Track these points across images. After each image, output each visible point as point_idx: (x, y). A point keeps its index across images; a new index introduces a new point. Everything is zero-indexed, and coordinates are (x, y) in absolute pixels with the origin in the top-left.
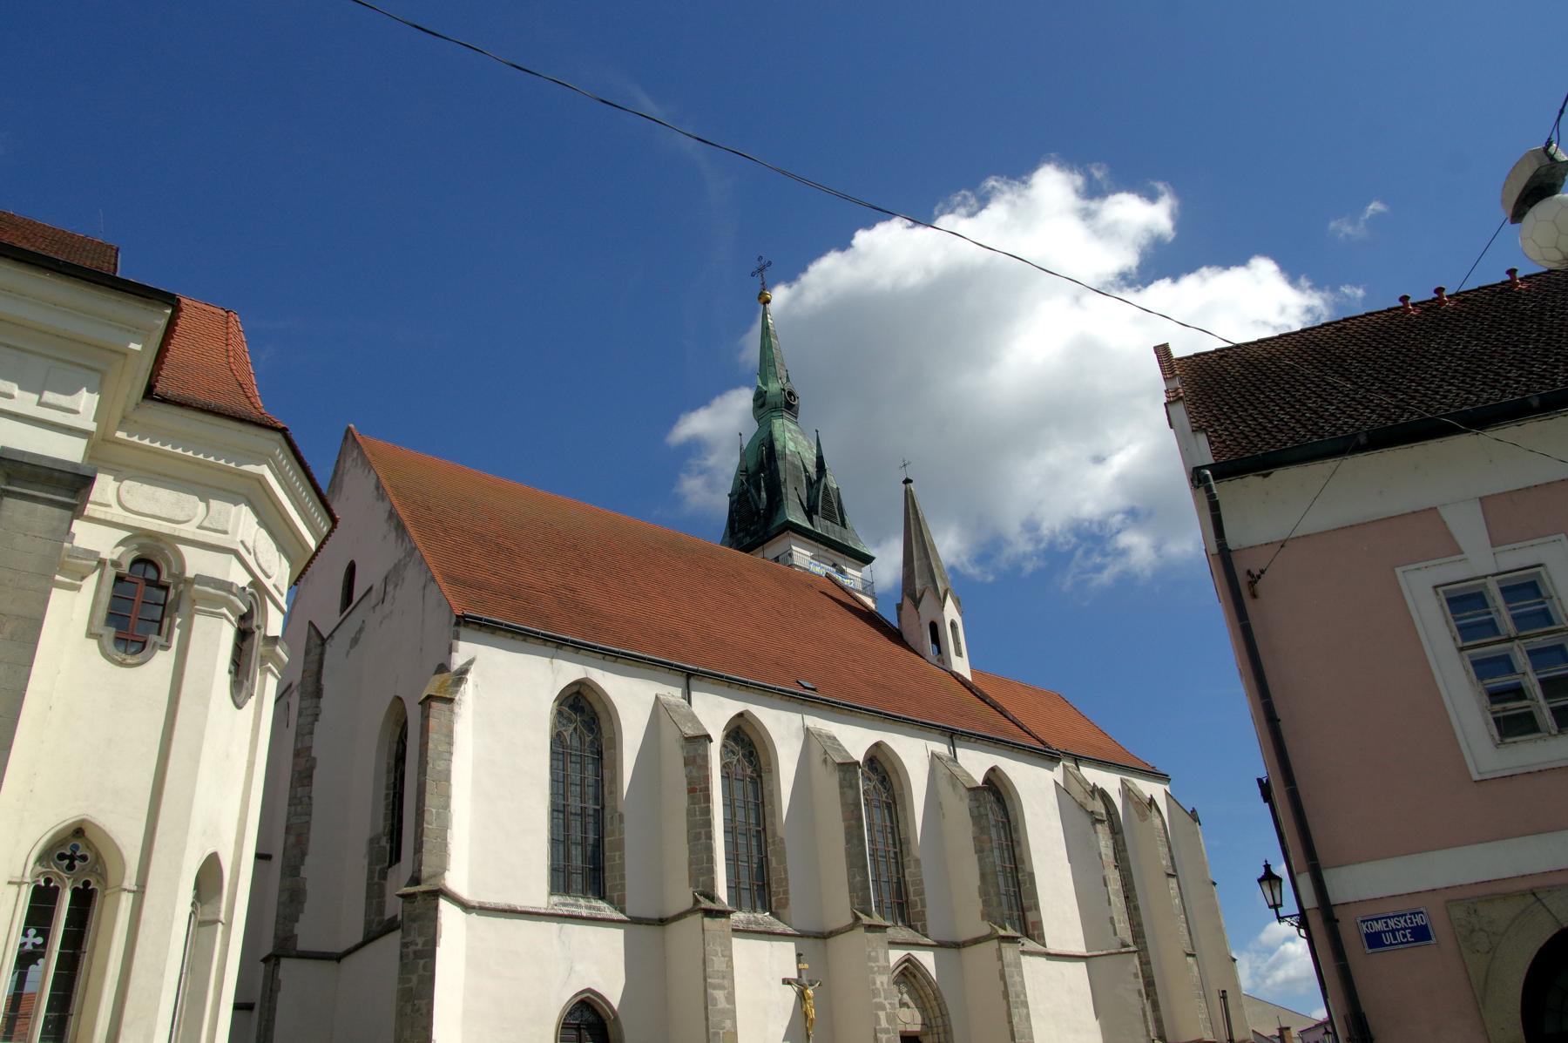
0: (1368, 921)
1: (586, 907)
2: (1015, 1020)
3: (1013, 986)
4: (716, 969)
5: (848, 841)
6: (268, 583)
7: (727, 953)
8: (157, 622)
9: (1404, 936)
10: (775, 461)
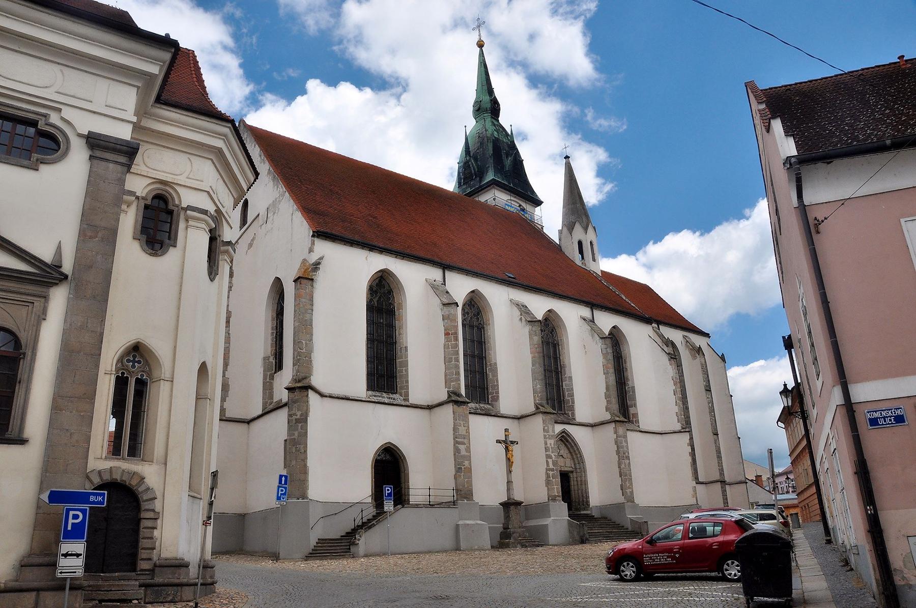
0: (871, 412)
1: (387, 397)
4: (460, 433)
6: (223, 210)
7: (466, 425)
8: (167, 232)
9: (890, 420)
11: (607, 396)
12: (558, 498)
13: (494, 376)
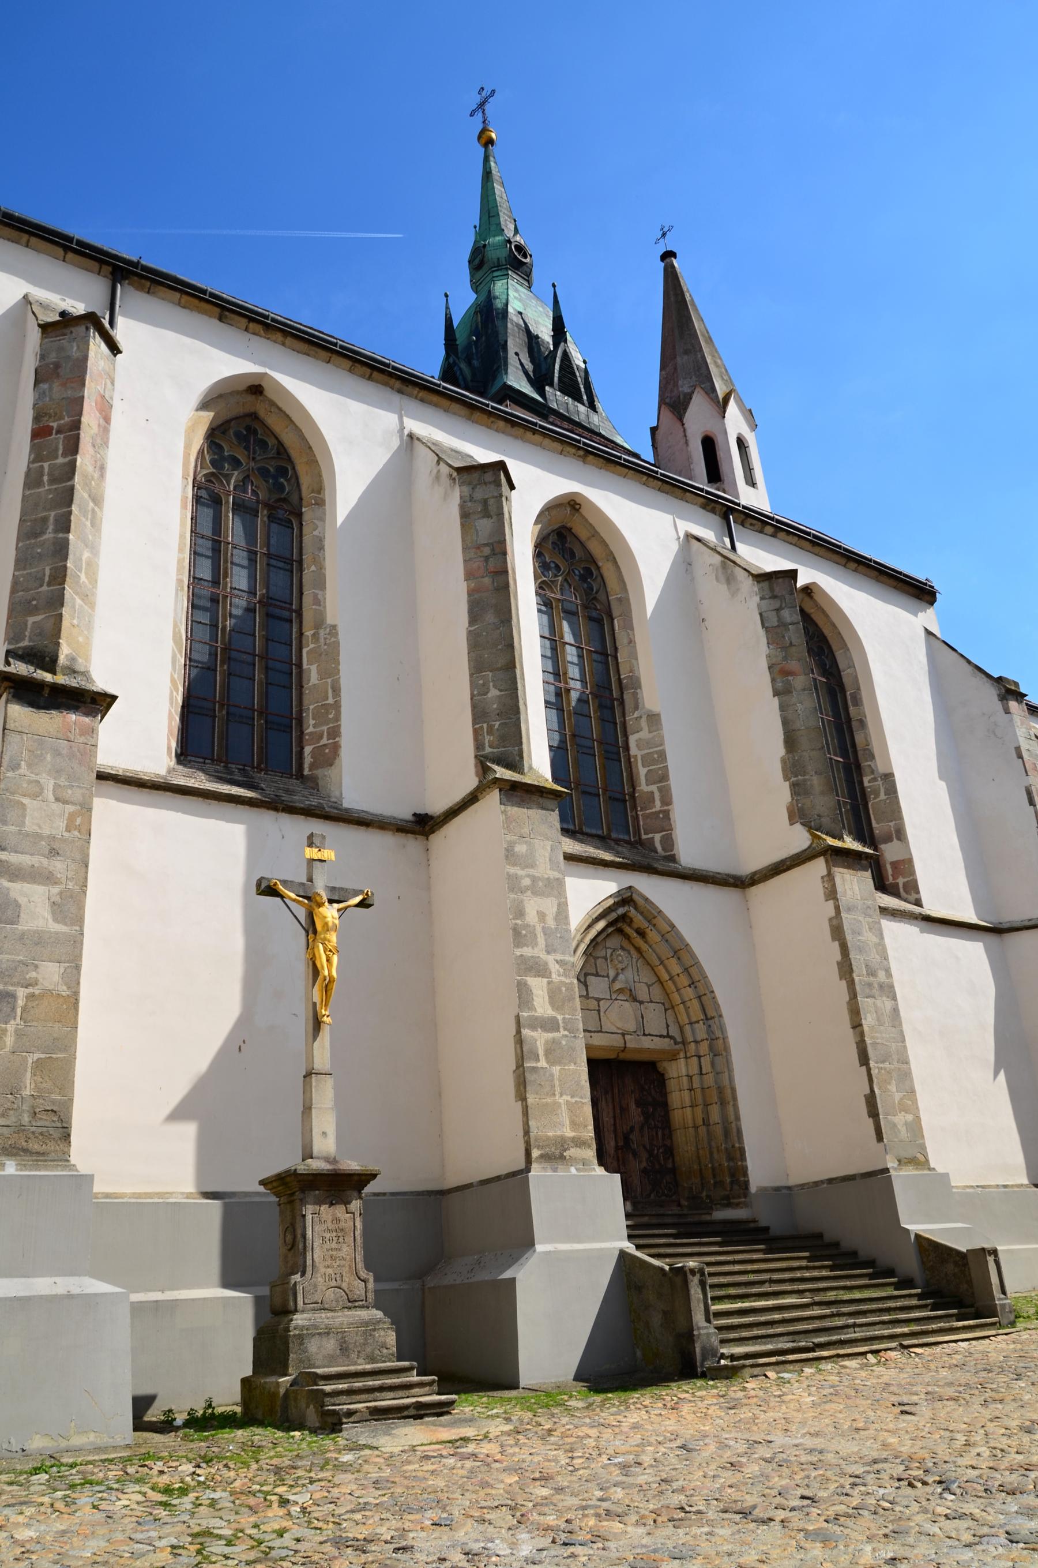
2: (868, 1022)
3: (860, 950)
4: (29, 826)
5: (474, 617)
10: (493, 322)
11: (792, 768)
12: (572, 1152)
13: (323, 675)
